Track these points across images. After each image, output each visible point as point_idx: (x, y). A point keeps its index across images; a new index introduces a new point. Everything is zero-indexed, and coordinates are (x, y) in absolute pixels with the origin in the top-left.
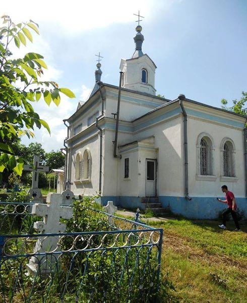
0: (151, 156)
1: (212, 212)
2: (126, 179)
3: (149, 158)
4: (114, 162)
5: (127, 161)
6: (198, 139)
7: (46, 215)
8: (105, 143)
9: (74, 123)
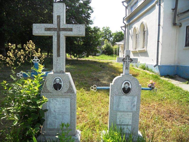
4: (173, 31)
8: (164, 11)
9: (131, 1)
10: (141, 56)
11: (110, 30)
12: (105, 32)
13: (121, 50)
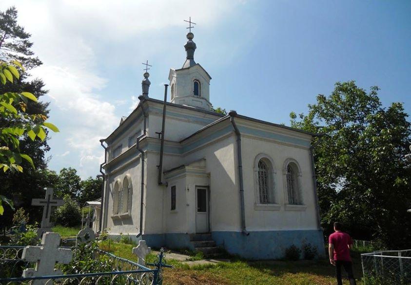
0: (202, 182)
1: (276, 250)
2: (173, 211)
3: (198, 185)
5: (174, 189)
6: (254, 163)
7: (39, 261)
8: (147, 168)
9: (113, 143)
10: (124, 224)
11: (76, 176)
12: (67, 178)
13: (96, 216)
